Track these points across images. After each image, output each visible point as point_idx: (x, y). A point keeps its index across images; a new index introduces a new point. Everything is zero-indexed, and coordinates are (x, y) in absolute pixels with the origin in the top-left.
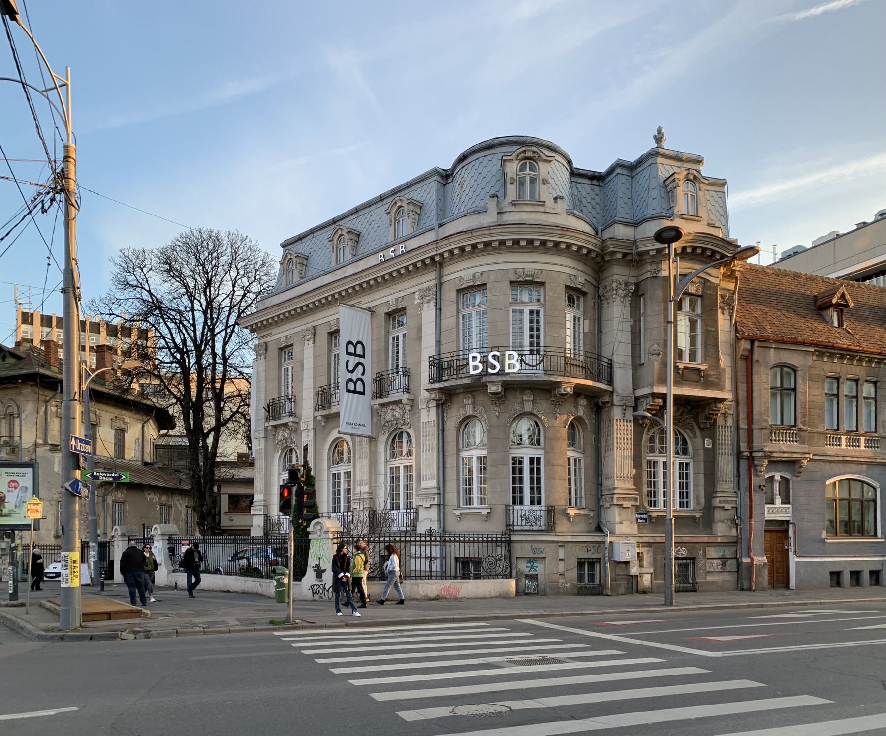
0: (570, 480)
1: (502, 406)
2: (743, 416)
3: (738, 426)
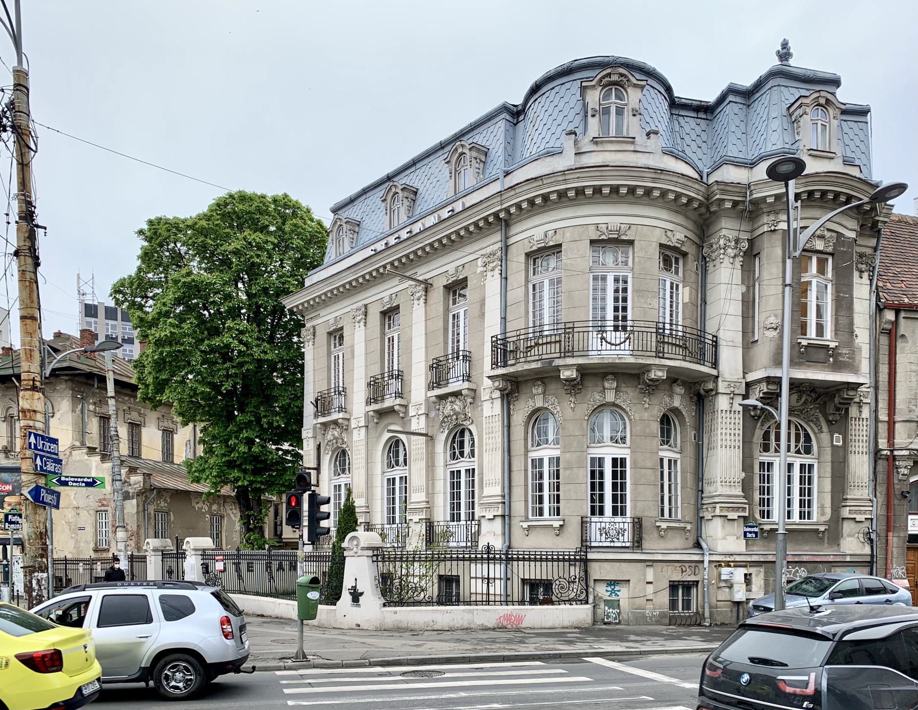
0: (662, 486)
1: (577, 396)
2: (883, 405)
3: (876, 418)
